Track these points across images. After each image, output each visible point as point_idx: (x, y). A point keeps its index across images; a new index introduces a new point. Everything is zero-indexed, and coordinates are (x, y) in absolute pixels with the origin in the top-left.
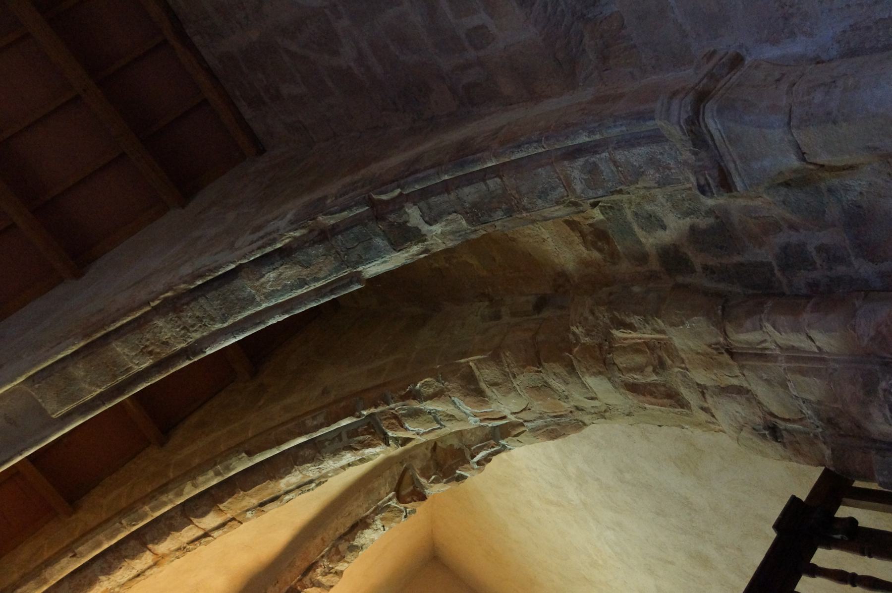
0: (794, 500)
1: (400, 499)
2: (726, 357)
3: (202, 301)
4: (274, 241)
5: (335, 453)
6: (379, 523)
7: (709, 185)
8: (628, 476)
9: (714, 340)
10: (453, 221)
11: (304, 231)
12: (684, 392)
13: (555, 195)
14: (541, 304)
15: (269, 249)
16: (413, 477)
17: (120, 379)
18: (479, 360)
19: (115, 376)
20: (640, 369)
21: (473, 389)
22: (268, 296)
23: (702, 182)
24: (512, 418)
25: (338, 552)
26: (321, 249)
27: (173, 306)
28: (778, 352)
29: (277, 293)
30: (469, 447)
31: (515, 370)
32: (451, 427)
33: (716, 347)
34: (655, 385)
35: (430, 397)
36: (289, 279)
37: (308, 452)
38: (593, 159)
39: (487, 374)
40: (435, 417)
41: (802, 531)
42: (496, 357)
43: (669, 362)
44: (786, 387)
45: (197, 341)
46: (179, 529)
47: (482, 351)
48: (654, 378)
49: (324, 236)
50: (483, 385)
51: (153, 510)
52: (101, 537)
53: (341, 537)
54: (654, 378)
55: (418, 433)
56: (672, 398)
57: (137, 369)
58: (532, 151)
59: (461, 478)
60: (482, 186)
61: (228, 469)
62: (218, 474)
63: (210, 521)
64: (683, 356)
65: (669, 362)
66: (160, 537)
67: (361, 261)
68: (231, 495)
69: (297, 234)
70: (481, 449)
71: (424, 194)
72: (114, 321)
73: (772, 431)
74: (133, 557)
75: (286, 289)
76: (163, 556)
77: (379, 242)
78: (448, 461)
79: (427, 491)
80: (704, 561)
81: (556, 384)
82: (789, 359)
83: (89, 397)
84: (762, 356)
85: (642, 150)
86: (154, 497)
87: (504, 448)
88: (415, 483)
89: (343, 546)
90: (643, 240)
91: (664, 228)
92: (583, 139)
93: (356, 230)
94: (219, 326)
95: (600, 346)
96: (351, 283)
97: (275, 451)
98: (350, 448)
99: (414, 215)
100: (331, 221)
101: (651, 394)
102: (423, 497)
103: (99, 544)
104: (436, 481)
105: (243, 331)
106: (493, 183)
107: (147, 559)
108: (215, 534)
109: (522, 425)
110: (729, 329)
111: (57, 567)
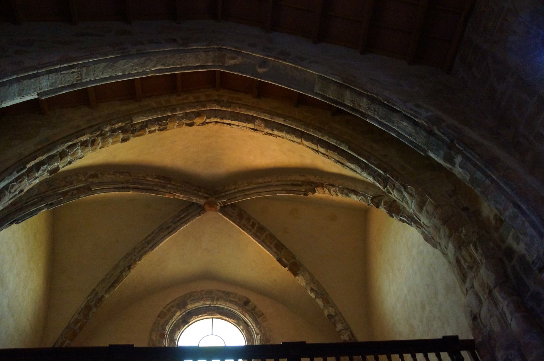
0: (457, 337)
1: (372, 200)
2: (487, 291)
3: (381, 108)
4: (417, 117)
5: (369, 174)
6: (360, 198)
7: (536, 264)
8: (432, 269)
9: (490, 284)
10: (467, 175)
11: (427, 125)
12: (468, 281)
13: (499, 207)
14: (466, 209)
15: (413, 118)
16: (381, 199)
17: (340, 100)
18: (431, 202)
19: (339, 99)
20: (466, 261)
21: (421, 206)
22: (398, 127)
23: (535, 262)
24: (422, 223)
25: (343, 191)
26: (425, 134)
27: (373, 100)
28: (501, 309)
29: (401, 128)
30: (403, 213)
31: (437, 216)
32: (404, 204)
33: (489, 287)
34: (464, 269)
35: (408, 193)
36: (408, 130)
37: (363, 165)
38: (519, 215)
39: (429, 207)
40: (404, 198)
41: (449, 344)
42: (436, 207)
43: (474, 270)
44: (491, 317)
45: (368, 115)
46: (313, 143)
47: (434, 200)
48: (466, 267)
49: (430, 133)
50: (424, 208)
51: (313, 132)
52: (294, 123)
53: (347, 189)
54: (466, 267)
55: (395, 195)
56: (463, 277)
57: (346, 103)
58: (508, 190)
59: (392, 216)
60: (484, 178)
61: (340, 145)
62: (336, 143)
63: (322, 150)
64: (479, 274)
65: (474, 270)
66: (306, 140)
67: (431, 150)
68: (334, 151)
69: (424, 123)
70: (406, 218)
71: (467, 159)
72: (354, 86)
73: (475, 318)
74: (296, 137)
75: (405, 131)
76: (303, 144)
77: (442, 153)
78: (394, 209)
79: (380, 207)
80: (423, 307)
81: (442, 231)
82: (500, 314)
83: (327, 96)
84: (496, 304)
85: (534, 233)
86: (316, 129)
87: (411, 225)
88: (380, 202)
89: (345, 191)
90: (509, 238)
91: (518, 244)
92: (524, 207)
93: (440, 142)
94: (378, 118)
95: (464, 242)
96: (422, 151)
97: (356, 156)
98: (374, 178)
99: (458, 159)
100: (437, 132)
101: (460, 269)
102: (378, 207)
103: (292, 125)
104: (385, 209)
105: (382, 126)
106: (488, 182)
107: (299, 140)
108: (320, 154)
109: (422, 227)
110: (497, 289)
111: (278, 119)
